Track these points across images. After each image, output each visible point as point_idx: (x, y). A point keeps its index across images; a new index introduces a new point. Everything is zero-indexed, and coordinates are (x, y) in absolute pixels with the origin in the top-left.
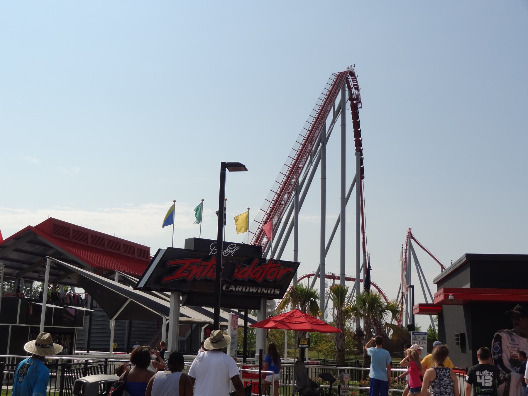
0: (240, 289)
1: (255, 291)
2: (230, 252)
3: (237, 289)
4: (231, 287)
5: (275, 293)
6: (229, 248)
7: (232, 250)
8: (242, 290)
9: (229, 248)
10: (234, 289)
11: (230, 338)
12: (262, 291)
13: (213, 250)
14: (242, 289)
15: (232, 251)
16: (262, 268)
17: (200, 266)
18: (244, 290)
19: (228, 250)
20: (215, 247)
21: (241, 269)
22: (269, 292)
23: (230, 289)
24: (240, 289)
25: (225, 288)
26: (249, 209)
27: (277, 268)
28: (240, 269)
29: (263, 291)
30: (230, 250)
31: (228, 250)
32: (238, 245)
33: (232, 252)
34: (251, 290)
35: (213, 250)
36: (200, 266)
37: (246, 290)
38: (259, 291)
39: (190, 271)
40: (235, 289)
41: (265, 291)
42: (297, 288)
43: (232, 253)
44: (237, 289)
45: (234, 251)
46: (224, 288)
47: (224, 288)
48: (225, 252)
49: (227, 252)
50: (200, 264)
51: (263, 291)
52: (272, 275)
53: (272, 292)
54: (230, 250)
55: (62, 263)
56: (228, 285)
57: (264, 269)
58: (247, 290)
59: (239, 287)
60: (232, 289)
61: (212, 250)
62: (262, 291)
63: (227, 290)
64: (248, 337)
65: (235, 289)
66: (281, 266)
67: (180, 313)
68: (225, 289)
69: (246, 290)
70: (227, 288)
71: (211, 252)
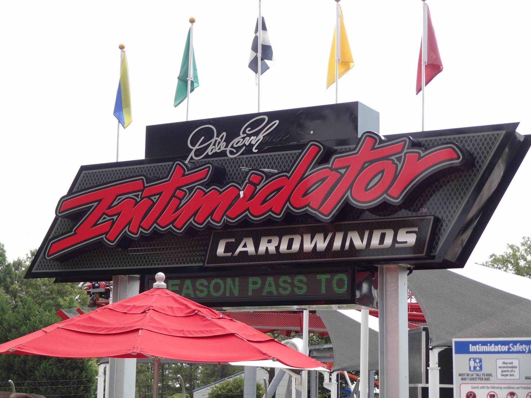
0: (272, 248)
1: (322, 245)
2: (247, 144)
3: (262, 249)
4: (242, 244)
5: (397, 245)
6: (244, 132)
7: (256, 134)
8: (277, 248)
9: (244, 132)
10: (250, 249)
11: (13, 385)
12: (348, 244)
13: (197, 147)
14: (277, 245)
15: (254, 140)
16: (336, 170)
17: (142, 199)
18: (283, 247)
19: (244, 138)
20: (203, 138)
21: (261, 185)
22: (375, 242)
23: (240, 249)
24: (272, 248)
25: (223, 250)
26: (122, 47)
27: (393, 158)
28: (259, 187)
29: (351, 241)
30: (250, 136)
31: (244, 138)
32: (272, 115)
33: (253, 143)
34: (308, 246)
35: (197, 147)
36: (142, 199)
37: (290, 246)
38: (337, 244)
39: (115, 218)
40: (257, 247)
41: (358, 243)
42: (438, 218)
43: (253, 145)
44: (262, 249)
45: (261, 137)
46: (221, 250)
47: (221, 250)
48: (232, 147)
49: (240, 144)
50: (140, 193)
51: (351, 241)
52: (369, 187)
53: (388, 241)
54: (247, 138)
55: (426, 174)
56: (233, 240)
57: (343, 171)
58: (296, 246)
59: (270, 241)
60: (245, 249)
61: (194, 149)
62: (348, 244)
63: (230, 254)
64: (171, 385)
65: (257, 247)
66: (405, 151)
67: (377, 317)
68: (224, 252)
69: (290, 246)
70: (230, 248)
71: (192, 154)
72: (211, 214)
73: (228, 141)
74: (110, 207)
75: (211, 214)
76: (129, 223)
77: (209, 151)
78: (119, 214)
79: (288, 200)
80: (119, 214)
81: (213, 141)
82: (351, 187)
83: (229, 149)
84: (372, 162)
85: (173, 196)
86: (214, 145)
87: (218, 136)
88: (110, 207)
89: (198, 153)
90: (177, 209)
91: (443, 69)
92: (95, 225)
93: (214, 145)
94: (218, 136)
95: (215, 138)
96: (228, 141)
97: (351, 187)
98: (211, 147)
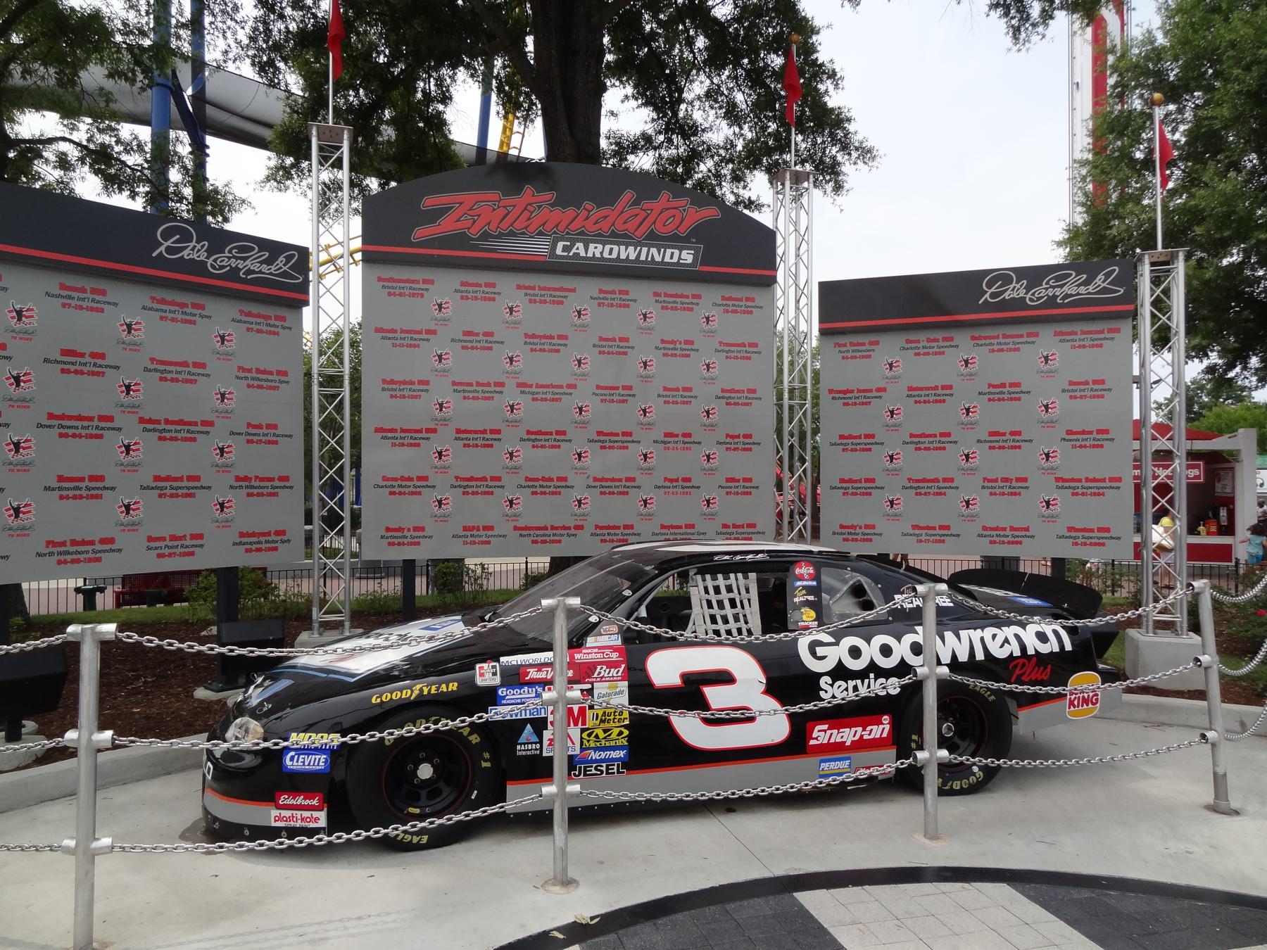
13: (993, 290)
19: (1047, 289)
23: (574, 250)
30: (1054, 287)
31: (1047, 289)
33: (1057, 294)
35: (993, 290)
40: (586, 250)
61: (990, 291)
65: (586, 250)
71: (987, 295)
72: (557, 226)
73: (1028, 289)
74: (471, 209)
75: (557, 226)
76: (489, 224)
77: (1006, 296)
78: (479, 216)
79: (613, 225)
80: (479, 216)
81: (1012, 286)
82: (654, 222)
83: (1029, 296)
84: (667, 209)
85: (525, 209)
86: (1013, 290)
87: (1017, 283)
88: (471, 209)
89: (993, 295)
90: (529, 219)
91: (769, 185)
92: (458, 221)
93: (1013, 290)
94: (1017, 283)
95: (1014, 284)
96: (1028, 289)
97: (654, 222)
98: (1008, 293)
